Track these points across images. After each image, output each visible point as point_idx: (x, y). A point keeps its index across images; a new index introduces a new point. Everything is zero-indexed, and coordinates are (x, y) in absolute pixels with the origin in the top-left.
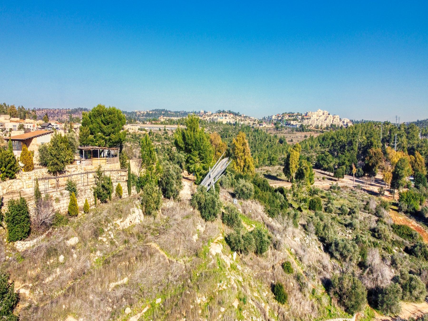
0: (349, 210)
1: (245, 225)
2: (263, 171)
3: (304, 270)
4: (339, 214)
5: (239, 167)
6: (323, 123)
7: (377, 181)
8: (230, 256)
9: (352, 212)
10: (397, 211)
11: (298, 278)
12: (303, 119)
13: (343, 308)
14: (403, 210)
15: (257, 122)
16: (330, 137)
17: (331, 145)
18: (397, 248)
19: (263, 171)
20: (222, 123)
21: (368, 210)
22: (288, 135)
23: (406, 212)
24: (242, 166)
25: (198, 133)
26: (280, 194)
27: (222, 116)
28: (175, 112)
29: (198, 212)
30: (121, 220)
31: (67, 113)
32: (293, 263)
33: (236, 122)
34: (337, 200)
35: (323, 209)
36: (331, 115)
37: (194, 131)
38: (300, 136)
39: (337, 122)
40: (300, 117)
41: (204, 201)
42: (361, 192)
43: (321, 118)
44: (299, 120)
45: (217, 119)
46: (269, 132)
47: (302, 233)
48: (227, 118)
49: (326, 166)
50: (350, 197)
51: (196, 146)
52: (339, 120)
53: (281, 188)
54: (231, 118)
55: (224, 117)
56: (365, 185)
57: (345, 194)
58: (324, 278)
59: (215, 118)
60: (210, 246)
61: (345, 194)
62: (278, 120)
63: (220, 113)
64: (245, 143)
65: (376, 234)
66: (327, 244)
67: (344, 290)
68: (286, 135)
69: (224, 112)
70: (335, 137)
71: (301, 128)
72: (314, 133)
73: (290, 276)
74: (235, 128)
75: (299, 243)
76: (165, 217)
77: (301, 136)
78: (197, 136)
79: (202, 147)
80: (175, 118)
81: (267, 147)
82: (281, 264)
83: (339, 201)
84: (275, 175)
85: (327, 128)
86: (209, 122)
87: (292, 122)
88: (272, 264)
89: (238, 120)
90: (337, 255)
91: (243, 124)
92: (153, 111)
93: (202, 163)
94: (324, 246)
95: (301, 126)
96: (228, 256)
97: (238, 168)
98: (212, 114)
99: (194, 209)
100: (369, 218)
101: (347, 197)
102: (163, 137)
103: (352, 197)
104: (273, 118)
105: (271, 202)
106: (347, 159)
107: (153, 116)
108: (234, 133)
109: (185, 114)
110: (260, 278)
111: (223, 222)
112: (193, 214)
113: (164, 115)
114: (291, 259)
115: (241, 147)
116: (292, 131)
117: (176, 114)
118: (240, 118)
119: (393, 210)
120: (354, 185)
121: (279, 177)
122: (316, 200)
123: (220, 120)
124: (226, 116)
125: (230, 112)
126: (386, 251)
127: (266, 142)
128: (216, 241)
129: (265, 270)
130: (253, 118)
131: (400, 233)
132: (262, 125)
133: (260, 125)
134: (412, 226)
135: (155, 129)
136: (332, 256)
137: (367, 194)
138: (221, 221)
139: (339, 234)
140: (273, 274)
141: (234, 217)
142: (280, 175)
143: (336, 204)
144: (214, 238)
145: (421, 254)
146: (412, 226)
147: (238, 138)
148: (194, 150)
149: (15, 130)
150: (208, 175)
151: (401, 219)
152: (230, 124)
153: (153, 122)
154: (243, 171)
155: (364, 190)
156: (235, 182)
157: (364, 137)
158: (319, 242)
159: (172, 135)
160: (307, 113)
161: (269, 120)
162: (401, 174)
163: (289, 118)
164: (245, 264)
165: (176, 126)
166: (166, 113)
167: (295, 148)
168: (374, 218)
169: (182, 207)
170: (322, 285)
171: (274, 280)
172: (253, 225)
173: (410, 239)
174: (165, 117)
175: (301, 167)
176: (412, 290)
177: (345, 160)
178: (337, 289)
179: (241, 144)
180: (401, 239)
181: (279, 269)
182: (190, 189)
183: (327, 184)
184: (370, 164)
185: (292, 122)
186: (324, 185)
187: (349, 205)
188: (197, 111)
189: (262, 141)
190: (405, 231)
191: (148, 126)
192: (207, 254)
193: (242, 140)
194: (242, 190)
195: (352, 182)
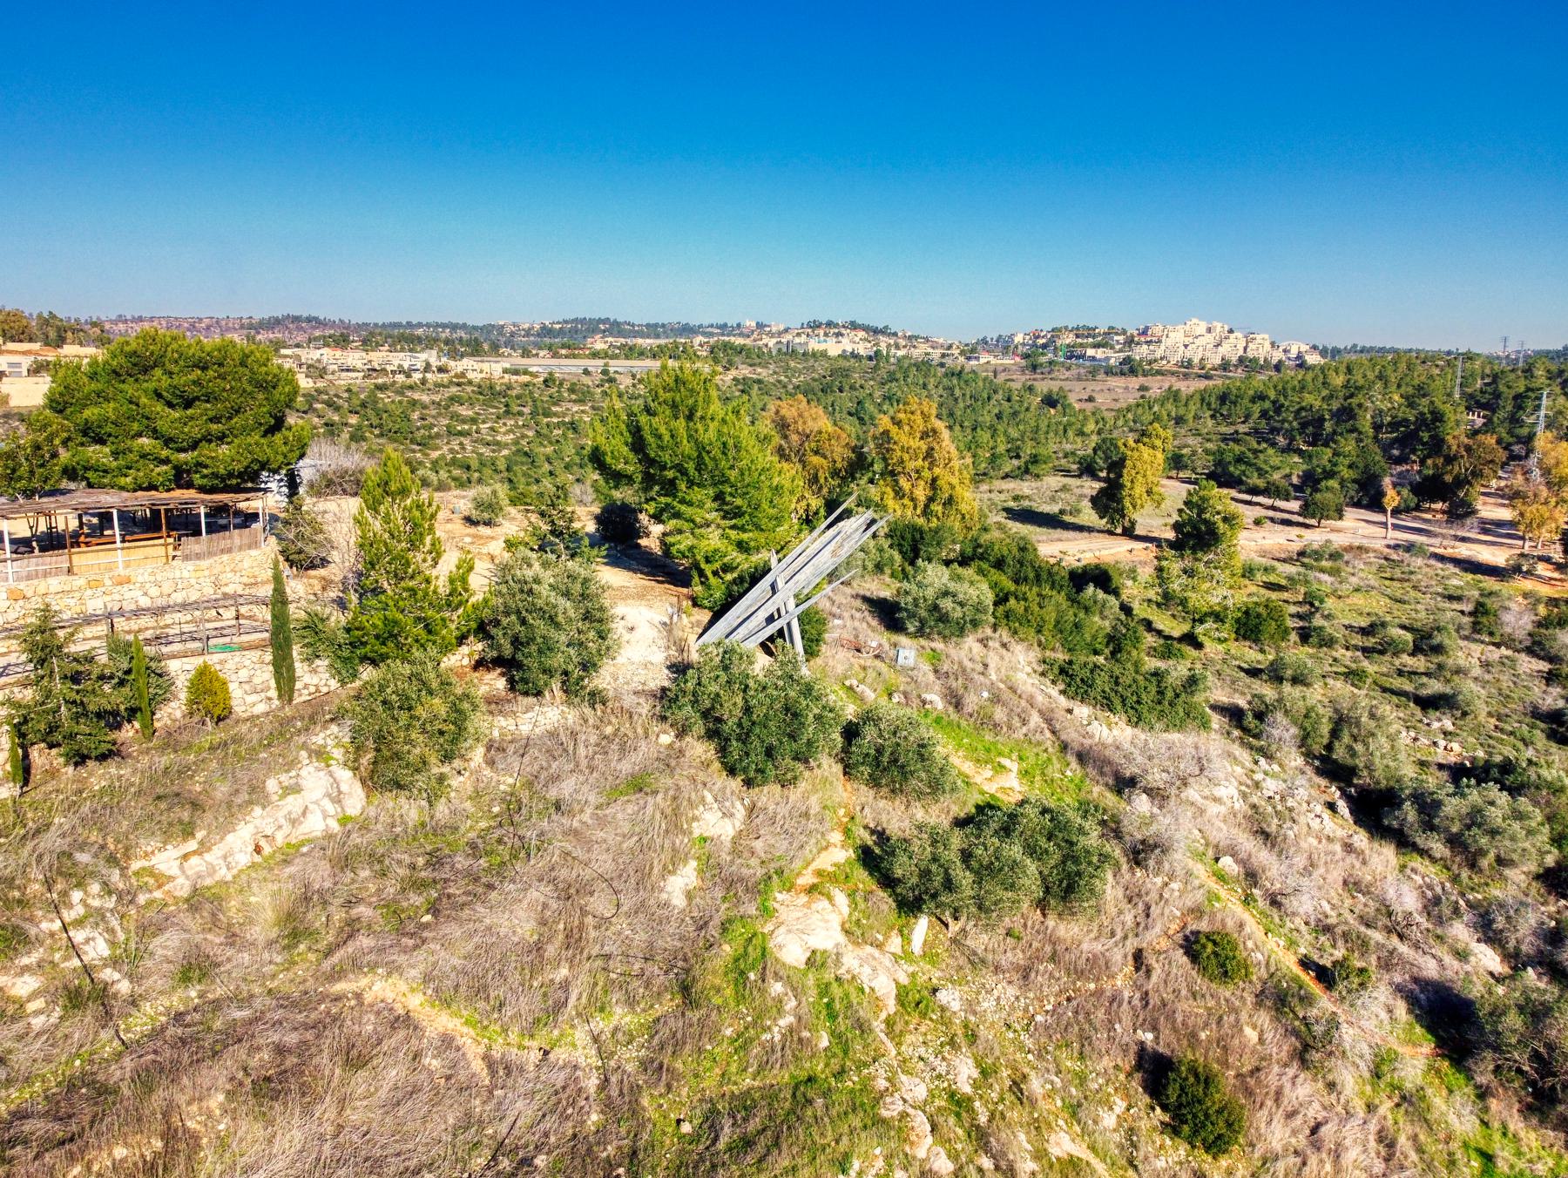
0: (1409, 637)
1: (967, 767)
3: (1303, 951)
4: (1365, 650)
5: (906, 501)
8: (895, 944)
11: (1279, 998)
12: (1130, 342)
15: (956, 352)
16: (1251, 392)
19: (995, 497)
20: (824, 354)
21: (1491, 634)
22: (1077, 386)
25: (713, 426)
26: (1101, 595)
27: (826, 335)
28: (648, 326)
29: (700, 750)
30: (192, 845)
31: (242, 327)
32: (1241, 925)
35: (1294, 637)
37: (690, 417)
38: (1123, 391)
39: (1261, 349)
40: (1121, 338)
45: (806, 344)
46: (1002, 377)
47: (1237, 750)
48: (845, 340)
49: (1255, 480)
50: (1387, 583)
51: (698, 469)
52: (1267, 345)
53: (1097, 567)
55: (832, 340)
58: (1416, 980)
59: (797, 340)
60: (766, 912)
61: (1362, 572)
62: (1034, 345)
63: (819, 326)
64: (934, 431)
68: (1067, 385)
69: (830, 324)
70: (1272, 394)
71: (1126, 368)
72: (1174, 379)
73: (1238, 995)
74: (876, 368)
75: (1239, 805)
76: (507, 782)
77: (1126, 388)
78: (709, 434)
79: (733, 475)
80: (648, 341)
81: (999, 416)
82: (1179, 938)
83: (1349, 601)
84: (1052, 509)
85: (1225, 366)
87: (1090, 352)
88: (1131, 945)
92: (566, 322)
93: (733, 527)
94: (1345, 795)
95: (1127, 360)
96: (879, 946)
98: (786, 330)
102: (599, 390)
103: (1395, 584)
104: (1019, 339)
105: (1068, 632)
106: (1347, 462)
107: (568, 337)
109: (464, 326)
110: (1073, 1030)
112: (670, 761)
114: (1232, 910)
115: (916, 443)
116: (1093, 373)
117: (653, 330)
120: (1392, 543)
121: (1067, 518)
122: (1261, 610)
123: (814, 345)
124: (839, 334)
125: (854, 326)
127: (993, 402)
128: (807, 879)
132: (977, 358)
133: (969, 359)
136: (1403, 843)
137: (1457, 570)
139: (1403, 749)
140: (1145, 997)
144: (797, 865)
148: (691, 484)
149: (19, 375)
150: (768, 580)
152: (854, 356)
153: (564, 352)
154: (926, 512)
157: (1396, 397)
158: (1323, 782)
160: (1147, 328)
161: (1004, 346)
164: (976, 962)
168: (1530, 665)
169: (609, 730)
170: (1411, 1018)
171: (1154, 1029)
172: (1006, 762)
183: (1279, 539)
184: (1448, 478)
185: (1090, 352)
186: (1261, 542)
187: (1396, 613)
188: (732, 322)
189: (976, 400)
191: (541, 364)
194: (936, 608)
195: (1380, 531)
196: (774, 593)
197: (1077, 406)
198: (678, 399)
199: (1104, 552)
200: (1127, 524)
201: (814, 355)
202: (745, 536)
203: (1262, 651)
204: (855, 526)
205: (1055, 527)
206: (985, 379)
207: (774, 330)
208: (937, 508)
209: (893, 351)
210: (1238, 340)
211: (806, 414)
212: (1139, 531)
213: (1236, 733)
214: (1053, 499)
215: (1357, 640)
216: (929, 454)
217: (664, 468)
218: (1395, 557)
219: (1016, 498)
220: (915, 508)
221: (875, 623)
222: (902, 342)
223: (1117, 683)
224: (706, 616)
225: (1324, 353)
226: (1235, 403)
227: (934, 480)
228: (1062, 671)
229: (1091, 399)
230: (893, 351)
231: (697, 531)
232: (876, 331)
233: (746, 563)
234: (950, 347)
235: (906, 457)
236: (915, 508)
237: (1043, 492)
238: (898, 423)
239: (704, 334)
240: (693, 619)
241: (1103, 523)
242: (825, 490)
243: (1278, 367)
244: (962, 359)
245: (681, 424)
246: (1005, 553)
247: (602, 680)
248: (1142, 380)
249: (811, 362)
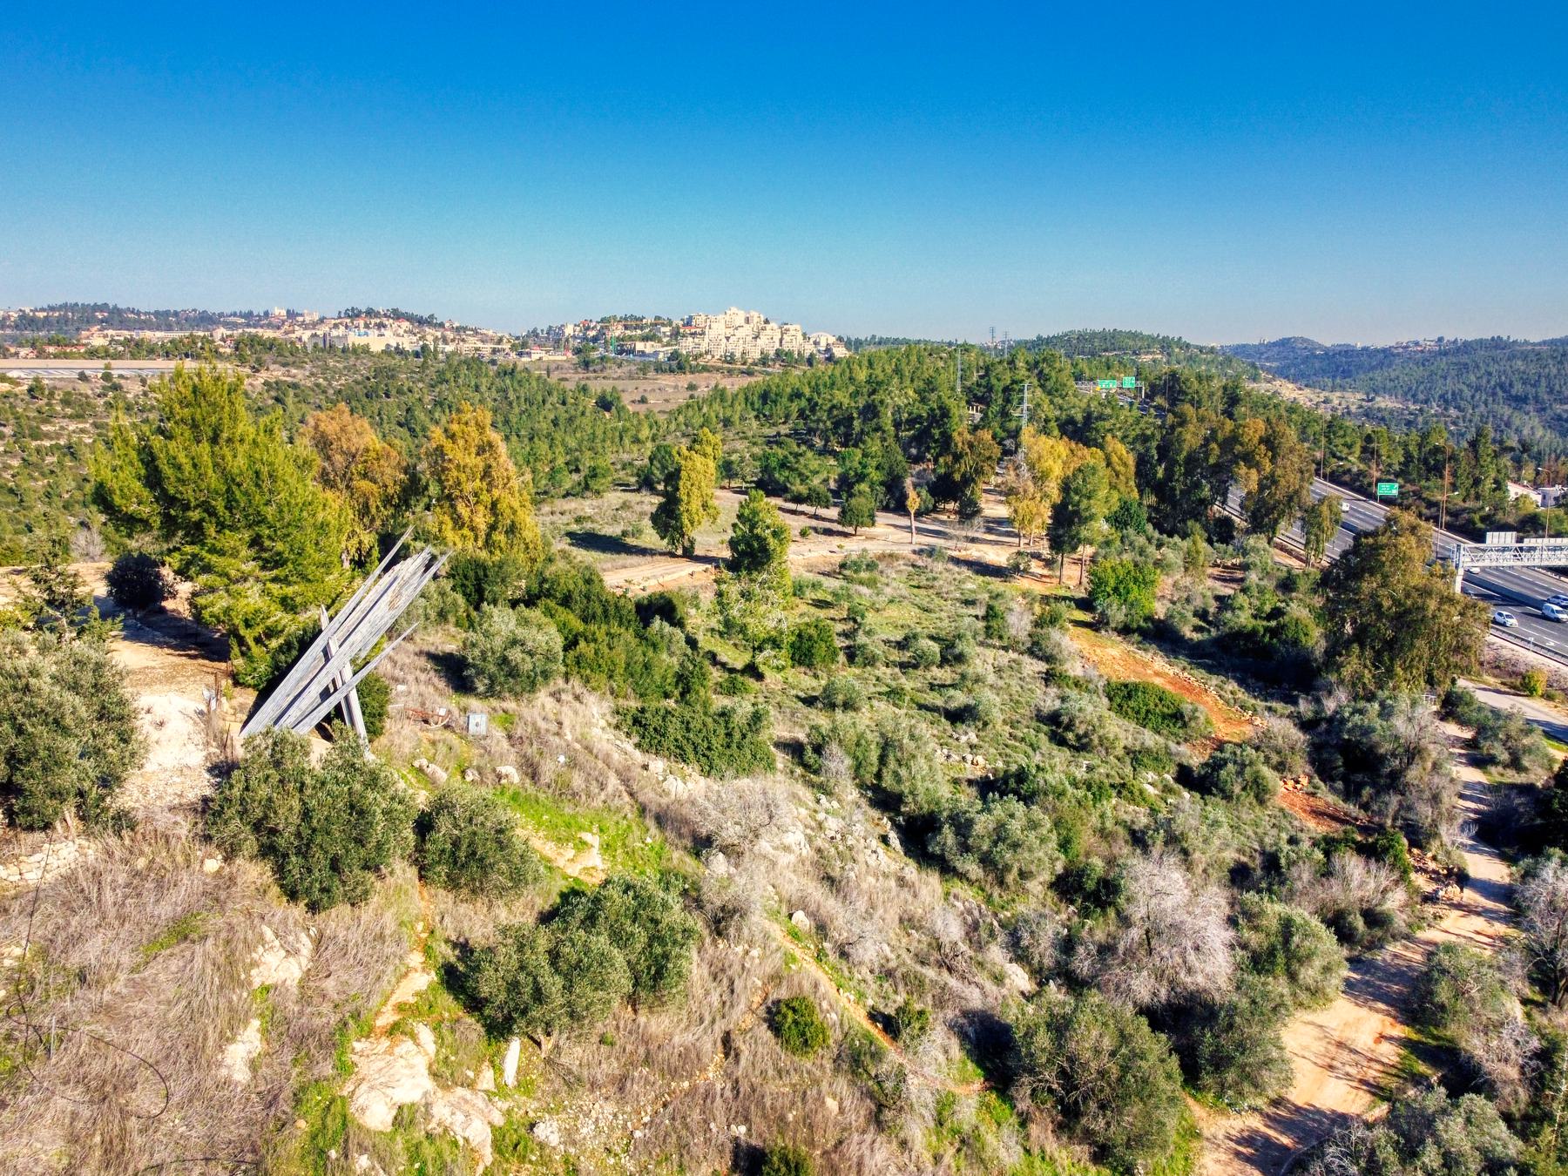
1: (549, 849)
2: (561, 521)
4: (903, 666)
5: (466, 531)
6: (748, 348)
7: (994, 525)
9: (951, 655)
10: (1093, 627)
11: (854, 1060)
12: (676, 334)
13: (1082, 1151)
14: (1113, 625)
15: (507, 346)
16: (789, 390)
17: (795, 415)
18: (1151, 776)
19: (561, 521)
20: (366, 350)
21: (1001, 638)
22: (630, 385)
23: (1125, 631)
24: (483, 527)
25: (241, 449)
26: (667, 628)
27: (367, 326)
28: (157, 313)
29: (255, 873)
33: (424, 348)
34: (878, 610)
36: (773, 325)
37: (214, 440)
38: (668, 391)
39: (795, 343)
40: (667, 330)
41: (295, 819)
42: (947, 570)
43: (740, 333)
44: (665, 340)
45: (345, 337)
48: (388, 332)
49: (798, 488)
51: (229, 508)
52: (800, 338)
53: (662, 596)
54: (401, 332)
55: (373, 333)
56: (950, 544)
57: (895, 581)
58: (965, 1014)
59: (335, 333)
61: (895, 581)
62: (585, 338)
63: (358, 316)
64: (490, 445)
65: (1070, 736)
66: (911, 819)
67: (1087, 1078)
68: (620, 385)
69: (370, 313)
70: (807, 391)
71: (674, 363)
72: (719, 376)
73: (817, 1063)
74: (424, 367)
77: (676, 387)
78: (238, 463)
79: (270, 512)
80: (159, 334)
81: (555, 423)
82: (762, 1012)
83: (886, 614)
84: (612, 530)
85: (764, 361)
86: (310, 350)
87: (640, 346)
88: (720, 1027)
89: (430, 338)
90: (973, 868)
91: (454, 353)
92: (52, 309)
93: (275, 580)
94: (896, 826)
95: (675, 356)
97: (464, 537)
98: (322, 320)
99: (230, 855)
100: (1015, 666)
101: (905, 592)
102: (101, 401)
103: (923, 592)
104: (569, 331)
106: (874, 464)
108: (421, 380)
111: (421, 877)
112: (218, 893)
113: (106, 323)
115: (473, 461)
116: (644, 370)
117: (163, 319)
118: (439, 334)
119: (1078, 623)
120: (917, 548)
121: (630, 541)
122: (812, 631)
123: (355, 339)
124: (381, 326)
125: (397, 315)
126: (1125, 798)
127: (548, 406)
128: (387, 1018)
129: (690, 1076)
130: (490, 333)
131: (1138, 713)
132: (529, 354)
133: (520, 354)
134: (1157, 674)
135: (66, 375)
138: (413, 872)
141: (486, 848)
142: (638, 532)
143: (882, 627)
145: (1244, 789)
146: (1157, 674)
147: (455, 427)
148: (221, 527)
151: (1115, 658)
152: (400, 351)
153: (51, 349)
154: (489, 544)
155: (957, 561)
156: (455, 603)
157: (911, 393)
158: (875, 814)
159: (145, 394)
160: (691, 318)
161: (555, 339)
162: (1087, 509)
163: (628, 332)
165: (161, 363)
166: (115, 317)
167: (697, 447)
168: (1034, 667)
171: (747, 1120)
172: (587, 837)
173: (1175, 730)
174: (110, 332)
175: (758, 531)
176: (1295, 966)
177: (865, 467)
178: (1049, 1075)
179: (474, 450)
180: (1150, 739)
181: (759, 1044)
182: (199, 738)
184: (957, 477)
185: (640, 346)
187: (926, 623)
188: (258, 310)
189: (531, 404)
190: (1152, 706)
192: (333, 1154)
193: (475, 434)
194: (505, 660)
195: (905, 536)
196: (327, 660)
197: (630, 408)
198: (198, 417)
199: (667, 578)
200: (687, 544)
201: (355, 351)
202: (289, 591)
203: (816, 676)
204: (412, 568)
205: (619, 552)
206: (539, 378)
207: (308, 319)
208: (499, 537)
209: (441, 346)
210: (773, 330)
211: (350, 428)
212: (698, 552)
213: (799, 771)
214: (615, 519)
215: (896, 656)
216: (486, 473)
217: (187, 507)
218: (920, 563)
219: (578, 520)
220: (476, 540)
221: (442, 684)
222: (450, 335)
223: (688, 730)
224: (250, 697)
225: (848, 344)
226: (775, 402)
227: (494, 505)
228: (636, 721)
229: (643, 401)
230: (441, 346)
231: (233, 587)
232: (421, 322)
233: (291, 625)
234: (500, 341)
235: (463, 477)
236: (476, 540)
237: (612, 509)
238: (452, 437)
239: (226, 325)
240: (235, 702)
241: (663, 544)
242: (378, 523)
243: (810, 361)
244: (513, 355)
245: (204, 448)
246: (572, 587)
247: (128, 797)
248: (689, 377)
249: (352, 360)
